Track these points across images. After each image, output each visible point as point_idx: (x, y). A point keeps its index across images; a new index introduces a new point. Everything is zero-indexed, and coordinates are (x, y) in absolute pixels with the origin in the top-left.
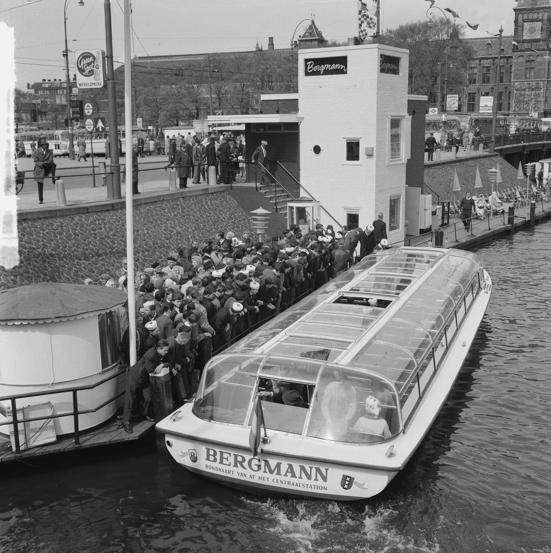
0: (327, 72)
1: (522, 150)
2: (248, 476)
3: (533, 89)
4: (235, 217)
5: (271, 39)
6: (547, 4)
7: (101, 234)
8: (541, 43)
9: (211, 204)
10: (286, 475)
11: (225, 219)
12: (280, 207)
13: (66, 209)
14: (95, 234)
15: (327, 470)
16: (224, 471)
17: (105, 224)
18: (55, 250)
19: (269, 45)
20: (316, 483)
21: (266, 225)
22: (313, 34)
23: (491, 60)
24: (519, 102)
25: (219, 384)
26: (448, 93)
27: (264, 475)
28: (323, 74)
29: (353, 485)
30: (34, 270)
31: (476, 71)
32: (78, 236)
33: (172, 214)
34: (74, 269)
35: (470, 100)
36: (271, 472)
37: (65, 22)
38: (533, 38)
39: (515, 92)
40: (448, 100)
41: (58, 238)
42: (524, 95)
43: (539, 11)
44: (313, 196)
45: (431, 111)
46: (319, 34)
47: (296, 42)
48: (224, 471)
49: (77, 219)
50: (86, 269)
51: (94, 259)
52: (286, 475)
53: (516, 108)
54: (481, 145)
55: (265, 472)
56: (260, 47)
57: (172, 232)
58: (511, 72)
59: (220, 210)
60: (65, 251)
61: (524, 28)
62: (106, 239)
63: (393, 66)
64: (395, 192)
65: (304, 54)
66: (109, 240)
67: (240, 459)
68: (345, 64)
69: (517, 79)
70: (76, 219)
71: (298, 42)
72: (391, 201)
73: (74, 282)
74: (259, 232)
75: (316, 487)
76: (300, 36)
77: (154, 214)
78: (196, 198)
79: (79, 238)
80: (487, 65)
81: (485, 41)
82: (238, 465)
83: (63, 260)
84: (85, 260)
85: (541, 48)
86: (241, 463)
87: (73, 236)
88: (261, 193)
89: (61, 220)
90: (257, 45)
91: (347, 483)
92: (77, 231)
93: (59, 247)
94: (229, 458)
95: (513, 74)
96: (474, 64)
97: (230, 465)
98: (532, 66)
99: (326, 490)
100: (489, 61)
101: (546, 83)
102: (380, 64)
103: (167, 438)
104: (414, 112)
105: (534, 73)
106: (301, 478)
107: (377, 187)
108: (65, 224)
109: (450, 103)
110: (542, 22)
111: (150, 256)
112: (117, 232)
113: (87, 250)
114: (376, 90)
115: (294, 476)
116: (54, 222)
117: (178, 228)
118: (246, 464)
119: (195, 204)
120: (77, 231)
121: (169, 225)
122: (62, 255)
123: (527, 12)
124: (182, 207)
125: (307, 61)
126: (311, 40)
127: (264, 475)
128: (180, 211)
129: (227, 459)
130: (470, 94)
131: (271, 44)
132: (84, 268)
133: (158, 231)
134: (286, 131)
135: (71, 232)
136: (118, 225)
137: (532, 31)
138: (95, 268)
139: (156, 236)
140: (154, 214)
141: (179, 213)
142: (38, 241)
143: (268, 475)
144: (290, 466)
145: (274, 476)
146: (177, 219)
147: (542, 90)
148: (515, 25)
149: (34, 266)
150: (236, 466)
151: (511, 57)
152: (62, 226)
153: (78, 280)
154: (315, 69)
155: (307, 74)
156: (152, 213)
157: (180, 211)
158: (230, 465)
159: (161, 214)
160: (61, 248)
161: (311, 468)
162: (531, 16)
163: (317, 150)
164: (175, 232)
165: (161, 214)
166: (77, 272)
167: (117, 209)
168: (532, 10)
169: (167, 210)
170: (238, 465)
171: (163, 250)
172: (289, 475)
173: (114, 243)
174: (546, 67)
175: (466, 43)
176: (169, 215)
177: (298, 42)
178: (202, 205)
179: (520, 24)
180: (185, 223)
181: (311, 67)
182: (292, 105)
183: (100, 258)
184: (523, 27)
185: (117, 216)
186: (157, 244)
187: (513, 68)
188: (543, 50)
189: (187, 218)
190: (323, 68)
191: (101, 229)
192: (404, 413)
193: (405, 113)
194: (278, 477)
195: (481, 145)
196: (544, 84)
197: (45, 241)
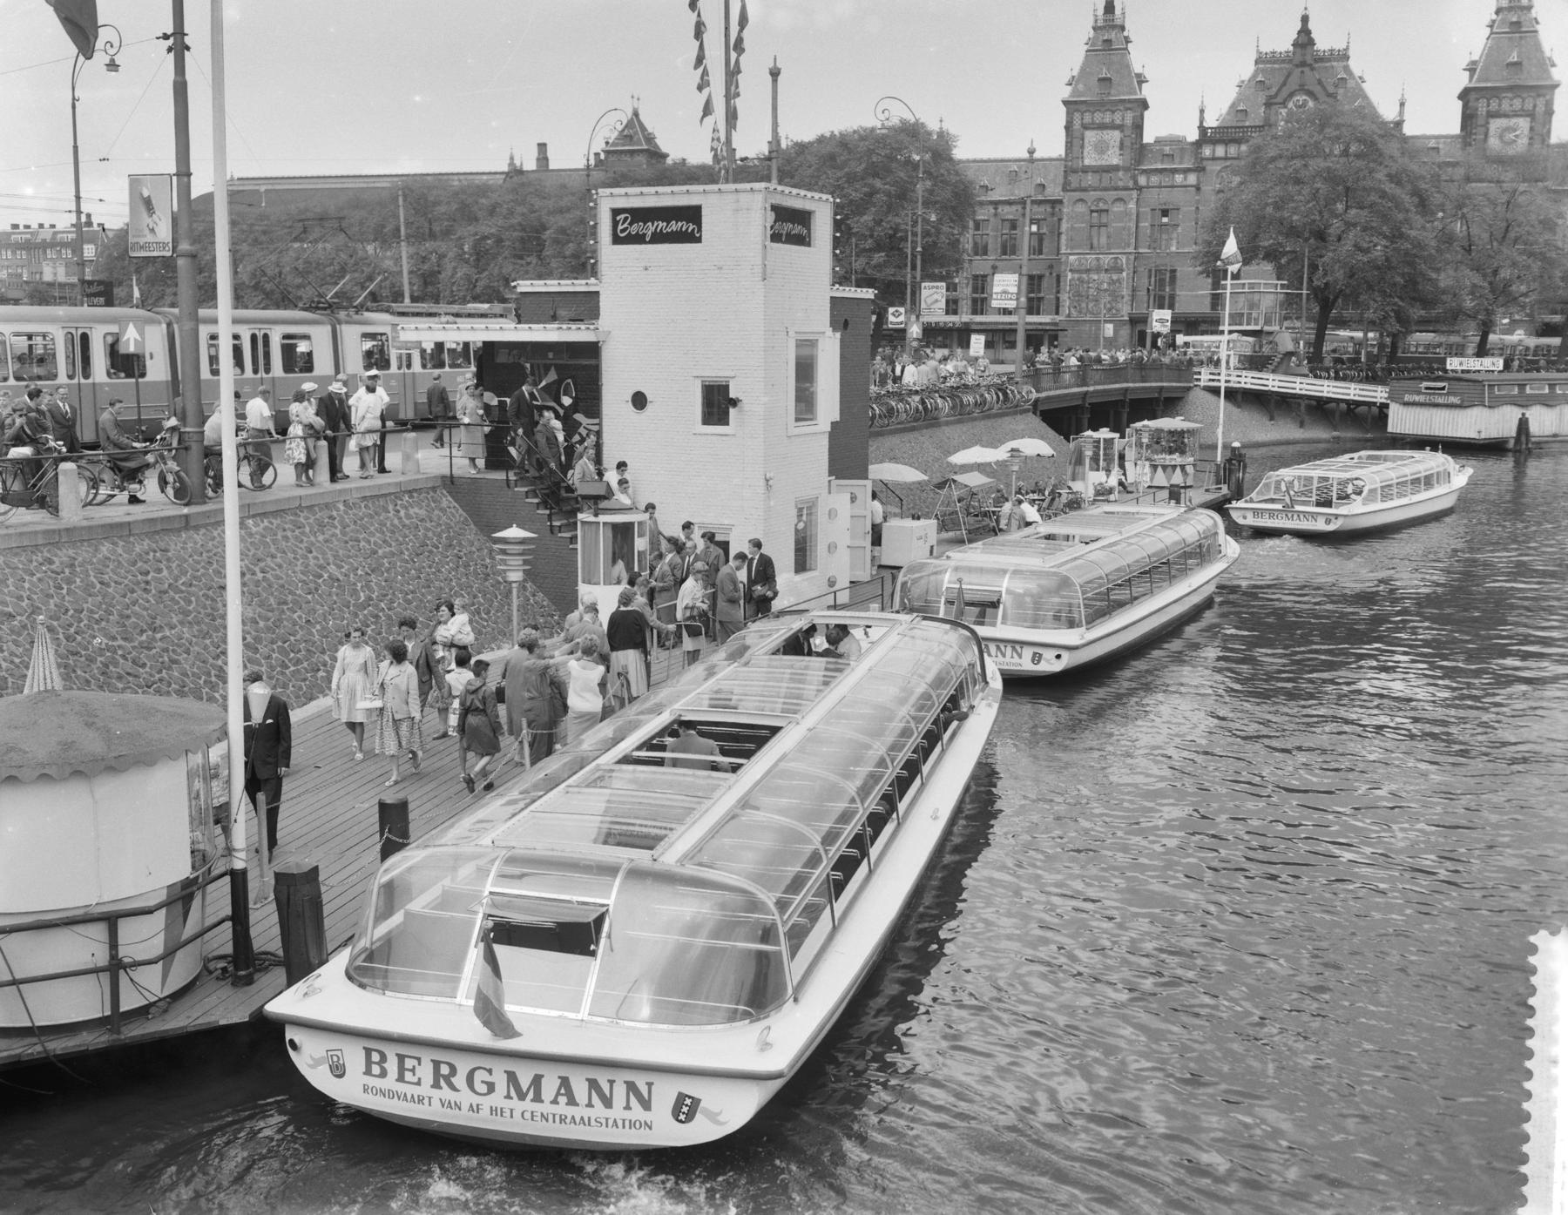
0: (659, 238)
1: (1080, 402)
2: (465, 1107)
5: (542, 147)
6: (1131, 94)
7: (159, 581)
8: (1121, 174)
9: (408, 516)
10: (555, 1102)
13: (83, 528)
14: (147, 583)
15: (650, 1085)
16: (409, 1097)
17: (169, 560)
18: (58, 619)
19: (538, 159)
20: (628, 1115)
24: (1078, 296)
25: (408, 914)
26: (923, 279)
27: (508, 1104)
29: (698, 1116)
30: (12, 662)
32: (108, 585)
33: (321, 538)
34: (99, 659)
35: (975, 290)
36: (522, 1096)
37: (74, 107)
38: (1104, 163)
39: (1070, 275)
40: (925, 293)
41: (64, 591)
45: (893, 314)
46: (650, 139)
47: (597, 155)
48: (409, 1097)
49: (105, 548)
50: (126, 659)
51: (144, 637)
52: (555, 1102)
55: (508, 1097)
57: (321, 576)
58: (1060, 234)
59: (427, 529)
60: (80, 621)
61: (1086, 141)
62: (172, 593)
63: (798, 229)
65: (609, 200)
66: (177, 597)
67: (445, 1070)
69: (1072, 248)
70: (104, 549)
71: (602, 156)
73: (101, 688)
75: (627, 1123)
76: (607, 143)
77: (279, 537)
79: (110, 590)
80: (1011, 217)
82: (442, 1083)
83: (75, 639)
84: (125, 639)
85: (1120, 184)
86: (447, 1079)
87: (98, 586)
89: (71, 552)
90: (512, 158)
91: (685, 1109)
92: (106, 577)
93: (67, 610)
95: (1063, 238)
97: (418, 1083)
98: (1104, 220)
99: (650, 1128)
100: (1014, 208)
101: (1132, 257)
103: (290, 1034)
104: (846, 324)
105: (1108, 237)
106: (590, 1105)
108: (80, 559)
109: (929, 302)
110: (1122, 131)
111: (269, 629)
112: (195, 577)
113: (128, 617)
115: (572, 1101)
116: (56, 555)
117: (332, 568)
118: (460, 1080)
119: (371, 517)
120: (106, 577)
121: (312, 562)
122: (72, 630)
124: (342, 522)
125: (616, 212)
126: (632, 152)
127: (508, 1104)
128: (338, 532)
129: (413, 1070)
130: (976, 277)
131: (543, 158)
132: (123, 656)
133: (287, 575)
135: (92, 578)
136: (198, 562)
137: (1101, 148)
138: (147, 657)
139: (283, 586)
140: (279, 537)
141: (333, 535)
142: (20, 598)
143: (515, 1103)
144: (565, 1082)
145: (528, 1105)
146: (331, 549)
147: (1124, 274)
148: (1067, 135)
149: (12, 654)
150: (436, 1085)
151: (1060, 202)
152: (72, 566)
153: (109, 684)
154: (634, 229)
155: (617, 240)
156: (275, 535)
157: (338, 532)
158: (418, 1083)
159: (296, 538)
160: (71, 612)
161: (611, 1082)
162: (1098, 117)
163: (639, 401)
164: (326, 576)
165: (296, 538)
166: (106, 666)
167: (197, 528)
168: (1100, 105)
169: (307, 529)
170: (442, 1083)
171: (300, 617)
172: (563, 1100)
173: (190, 602)
174: (1133, 225)
176: (312, 539)
178: (387, 518)
179: (1076, 134)
180: (349, 557)
182: (586, 307)
183: (159, 636)
184: (1083, 139)
185: (196, 543)
186: (285, 603)
187: (1064, 226)
188: (1126, 189)
190: (650, 228)
191: (159, 571)
192: (794, 970)
194: (537, 1107)
196: (1128, 259)
197: (35, 597)
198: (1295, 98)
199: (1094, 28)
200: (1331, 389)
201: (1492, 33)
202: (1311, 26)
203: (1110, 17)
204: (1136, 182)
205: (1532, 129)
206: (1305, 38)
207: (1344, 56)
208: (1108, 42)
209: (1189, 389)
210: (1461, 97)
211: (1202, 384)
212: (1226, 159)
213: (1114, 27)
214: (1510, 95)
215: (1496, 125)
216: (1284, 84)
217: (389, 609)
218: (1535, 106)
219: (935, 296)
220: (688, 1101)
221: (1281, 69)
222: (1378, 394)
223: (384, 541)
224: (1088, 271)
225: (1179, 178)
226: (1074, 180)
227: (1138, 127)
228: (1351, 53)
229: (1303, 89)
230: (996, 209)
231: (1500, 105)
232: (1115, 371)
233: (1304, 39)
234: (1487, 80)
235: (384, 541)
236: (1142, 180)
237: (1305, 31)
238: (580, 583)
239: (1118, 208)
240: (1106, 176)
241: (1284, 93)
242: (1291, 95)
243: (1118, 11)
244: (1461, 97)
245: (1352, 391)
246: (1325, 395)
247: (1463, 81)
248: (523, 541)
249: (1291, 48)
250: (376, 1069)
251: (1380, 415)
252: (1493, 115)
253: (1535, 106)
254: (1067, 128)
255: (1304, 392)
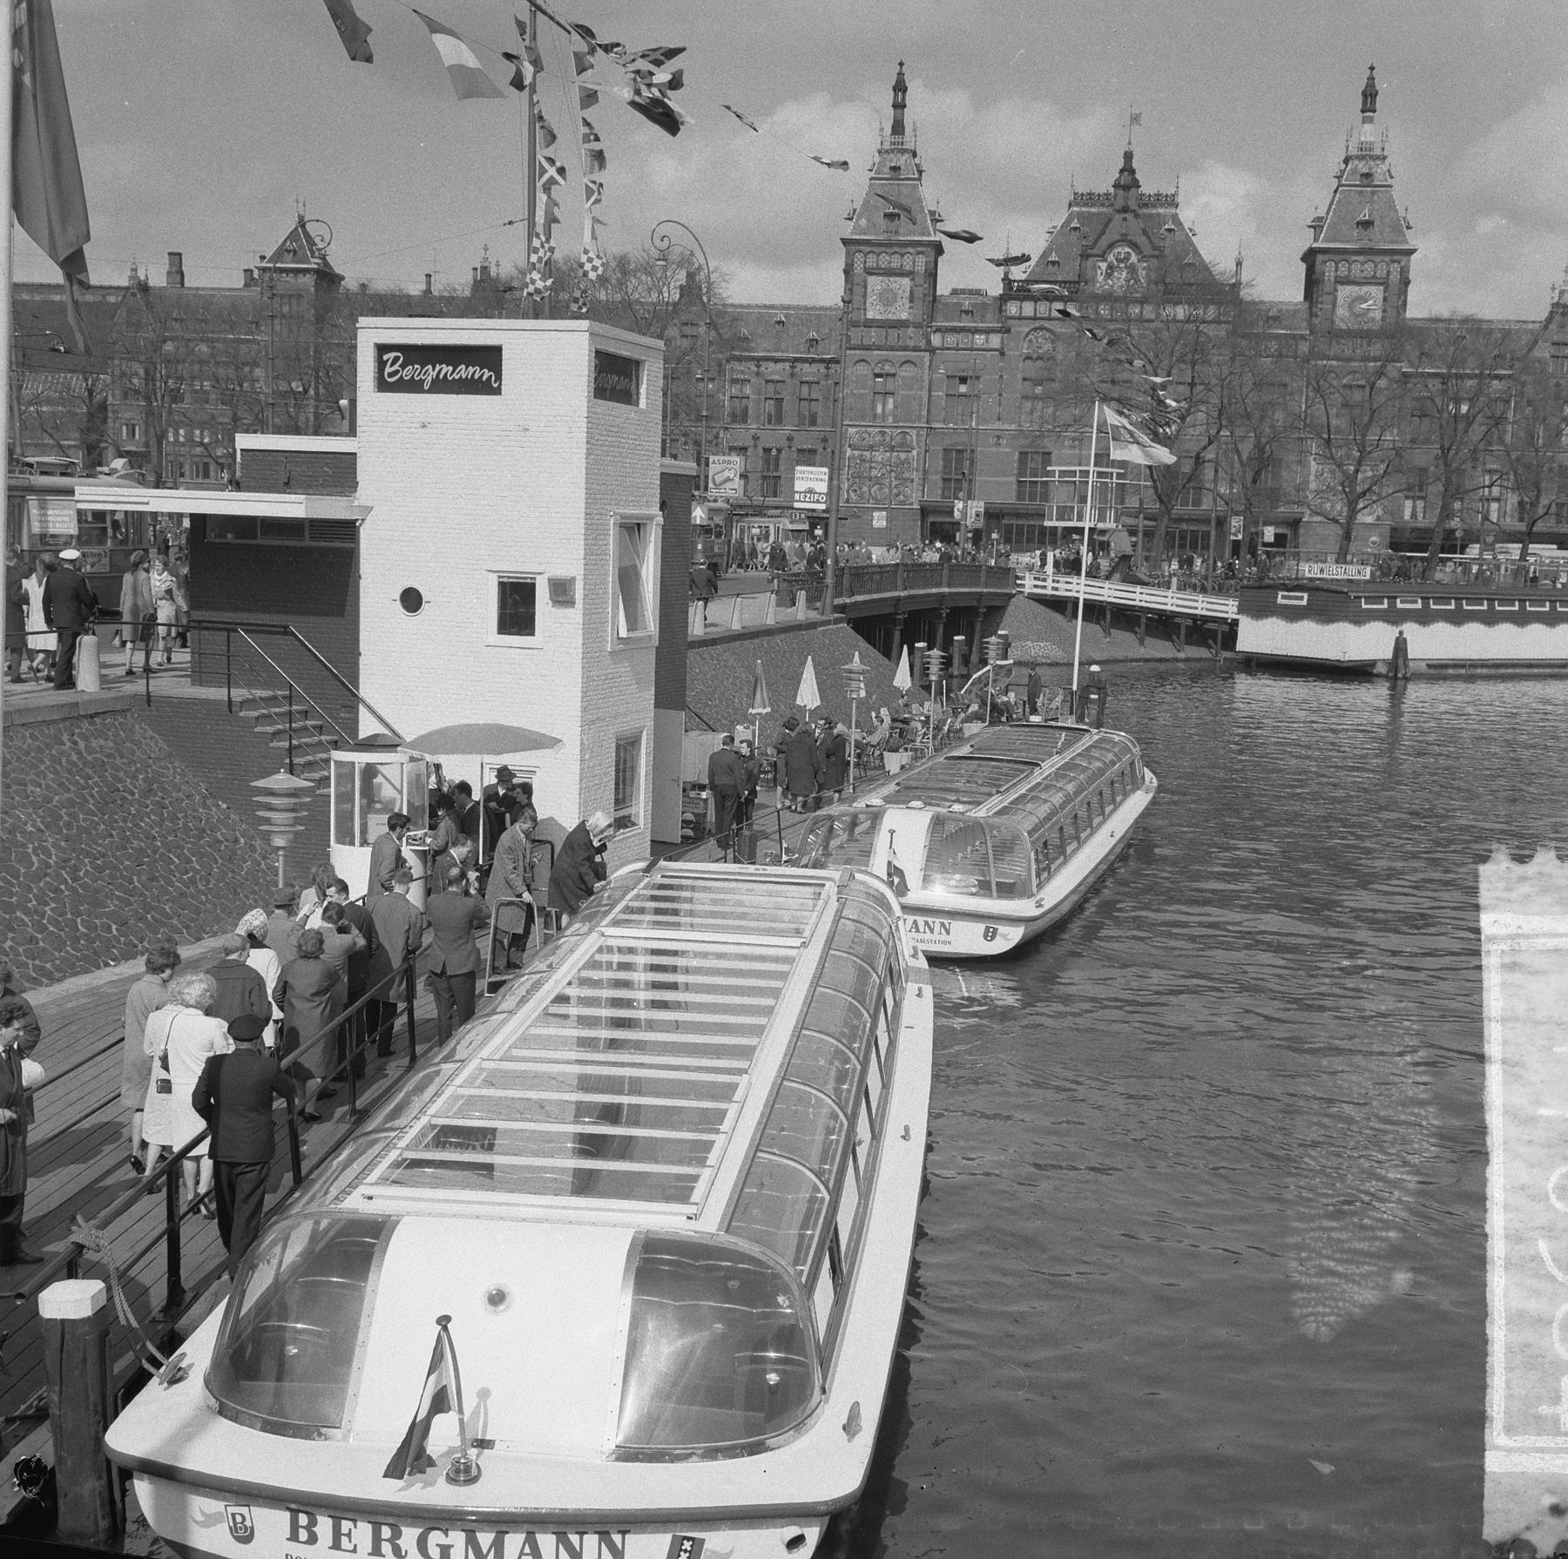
0: (441, 386)
3: (892, 449)
4: (163, 790)
5: (176, 257)
8: (911, 331)
9: (90, 750)
11: (133, 794)
12: (302, 760)
19: (169, 273)
21: (297, 821)
22: (300, 253)
23: (787, 365)
28: (429, 391)
31: (748, 390)
38: (890, 316)
42: (871, 461)
43: (903, 250)
44: (395, 727)
53: (852, 495)
54: (802, 596)
56: (143, 278)
61: (869, 289)
64: (625, 726)
68: (496, 366)
72: (618, 747)
74: (279, 841)
78: (41, 732)
81: (770, 315)
85: (911, 343)
88: (245, 720)
94: (353, 1530)
96: (742, 372)
98: (890, 388)
100: (780, 366)
101: (924, 432)
102: (593, 375)
107: (584, 710)
109: (718, 479)
110: (913, 279)
114: (584, 446)
123: (876, 249)
125: (382, 349)
129: (349, 1535)
134: (314, 544)
137: (888, 298)
147: (914, 453)
148: (846, 281)
154: (407, 373)
155: (383, 385)
162: (884, 260)
163: (412, 600)
175: (735, 319)
177: (256, 274)
178: (62, 753)
181: (396, 367)
184: (865, 287)
188: (916, 349)
189: (16, 792)
190: (430, 373)
193: (655, 510)
195: (802, 596)
196: (918, 435)
198: (1116, 251)
199: (879, 152)
200: (1144, 597)
201: (1340, 185)
202: (1135, 164)
203: (898, 138)
204: (929, 342)
205: (1385, 299)
206: (1128, 178)
207: (1171, 202)
208: (895, 169)
209: (1011, 596)
210: (1303, 259)
211: (1027, 590)
212: (1035, 318)
213: (903, 151)
214: (1361, 258)
215: (1344, 292)
216: (1103, 233)
217: (75, 880)
218: (1389, 273)
219: (727, 474)
220: (687, 1545)
221: (1099, 214)
222: (1227, 608)
223: (61, 785)
224: (871, 448)
225: (979, 339)
226: (856, 335)
227: (932, 275)
228: (1180, 199)
229: (1125, 240)
230: (758, 366)
231: (1349, 271)
232: (885, 574)
233: (1125, 179)
234: (1335, 240)
235: (61, 785)
236: (936, 340)
237: (1128, 169)
238: (332, 843)
239: (906, 372)
240: (894, 333)
241: (1104, 242)
242: (1111, 246)
243: (908, 130)
244: (1303, 259)
245: (1202, 605)
246: (1168, 608)
247: (1306, 241)
248: (294, 793)
249: (1112, 190)
250: (303, 1535)
251: (1230, 632)
252: (1347, 281)
253: (1389, 273)
254: (846, 272)
255: (1143, 604)
